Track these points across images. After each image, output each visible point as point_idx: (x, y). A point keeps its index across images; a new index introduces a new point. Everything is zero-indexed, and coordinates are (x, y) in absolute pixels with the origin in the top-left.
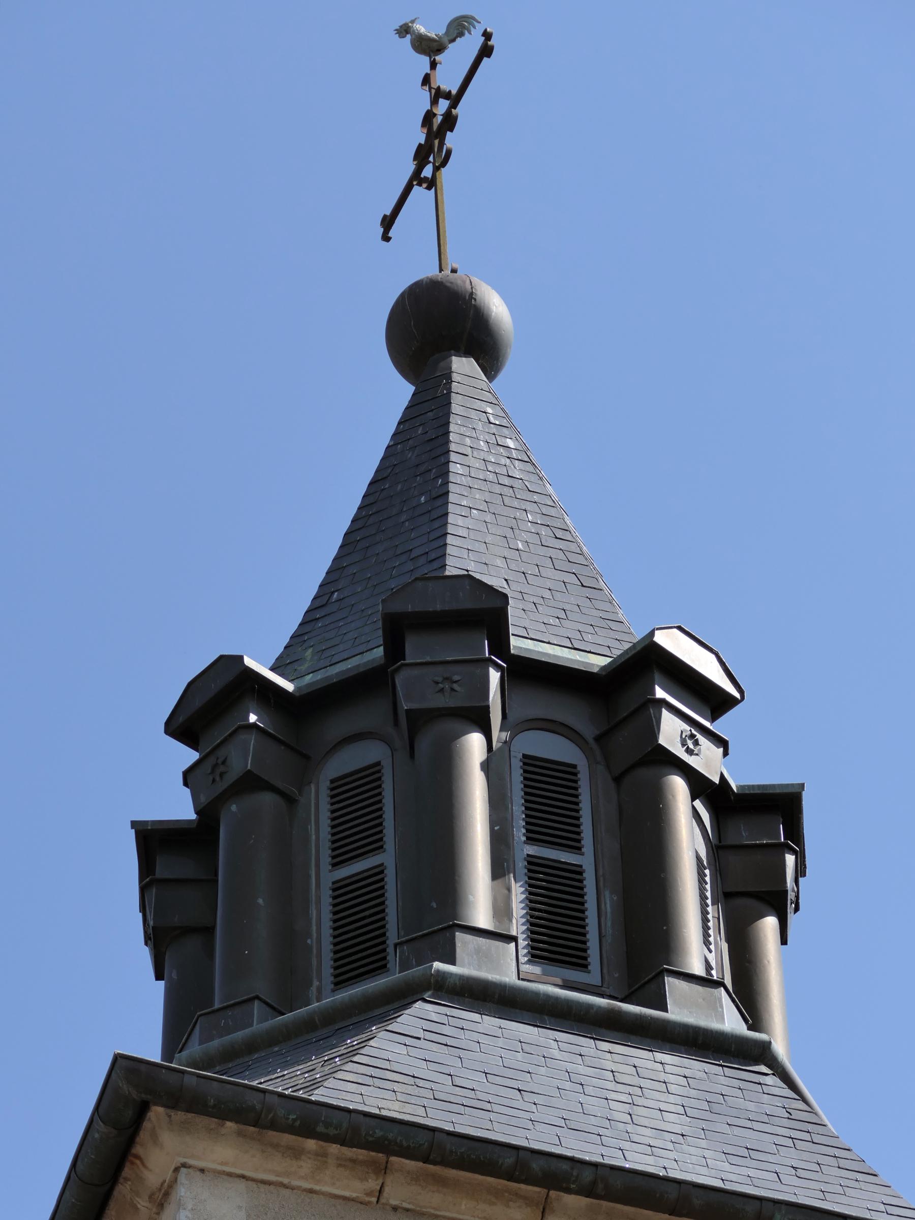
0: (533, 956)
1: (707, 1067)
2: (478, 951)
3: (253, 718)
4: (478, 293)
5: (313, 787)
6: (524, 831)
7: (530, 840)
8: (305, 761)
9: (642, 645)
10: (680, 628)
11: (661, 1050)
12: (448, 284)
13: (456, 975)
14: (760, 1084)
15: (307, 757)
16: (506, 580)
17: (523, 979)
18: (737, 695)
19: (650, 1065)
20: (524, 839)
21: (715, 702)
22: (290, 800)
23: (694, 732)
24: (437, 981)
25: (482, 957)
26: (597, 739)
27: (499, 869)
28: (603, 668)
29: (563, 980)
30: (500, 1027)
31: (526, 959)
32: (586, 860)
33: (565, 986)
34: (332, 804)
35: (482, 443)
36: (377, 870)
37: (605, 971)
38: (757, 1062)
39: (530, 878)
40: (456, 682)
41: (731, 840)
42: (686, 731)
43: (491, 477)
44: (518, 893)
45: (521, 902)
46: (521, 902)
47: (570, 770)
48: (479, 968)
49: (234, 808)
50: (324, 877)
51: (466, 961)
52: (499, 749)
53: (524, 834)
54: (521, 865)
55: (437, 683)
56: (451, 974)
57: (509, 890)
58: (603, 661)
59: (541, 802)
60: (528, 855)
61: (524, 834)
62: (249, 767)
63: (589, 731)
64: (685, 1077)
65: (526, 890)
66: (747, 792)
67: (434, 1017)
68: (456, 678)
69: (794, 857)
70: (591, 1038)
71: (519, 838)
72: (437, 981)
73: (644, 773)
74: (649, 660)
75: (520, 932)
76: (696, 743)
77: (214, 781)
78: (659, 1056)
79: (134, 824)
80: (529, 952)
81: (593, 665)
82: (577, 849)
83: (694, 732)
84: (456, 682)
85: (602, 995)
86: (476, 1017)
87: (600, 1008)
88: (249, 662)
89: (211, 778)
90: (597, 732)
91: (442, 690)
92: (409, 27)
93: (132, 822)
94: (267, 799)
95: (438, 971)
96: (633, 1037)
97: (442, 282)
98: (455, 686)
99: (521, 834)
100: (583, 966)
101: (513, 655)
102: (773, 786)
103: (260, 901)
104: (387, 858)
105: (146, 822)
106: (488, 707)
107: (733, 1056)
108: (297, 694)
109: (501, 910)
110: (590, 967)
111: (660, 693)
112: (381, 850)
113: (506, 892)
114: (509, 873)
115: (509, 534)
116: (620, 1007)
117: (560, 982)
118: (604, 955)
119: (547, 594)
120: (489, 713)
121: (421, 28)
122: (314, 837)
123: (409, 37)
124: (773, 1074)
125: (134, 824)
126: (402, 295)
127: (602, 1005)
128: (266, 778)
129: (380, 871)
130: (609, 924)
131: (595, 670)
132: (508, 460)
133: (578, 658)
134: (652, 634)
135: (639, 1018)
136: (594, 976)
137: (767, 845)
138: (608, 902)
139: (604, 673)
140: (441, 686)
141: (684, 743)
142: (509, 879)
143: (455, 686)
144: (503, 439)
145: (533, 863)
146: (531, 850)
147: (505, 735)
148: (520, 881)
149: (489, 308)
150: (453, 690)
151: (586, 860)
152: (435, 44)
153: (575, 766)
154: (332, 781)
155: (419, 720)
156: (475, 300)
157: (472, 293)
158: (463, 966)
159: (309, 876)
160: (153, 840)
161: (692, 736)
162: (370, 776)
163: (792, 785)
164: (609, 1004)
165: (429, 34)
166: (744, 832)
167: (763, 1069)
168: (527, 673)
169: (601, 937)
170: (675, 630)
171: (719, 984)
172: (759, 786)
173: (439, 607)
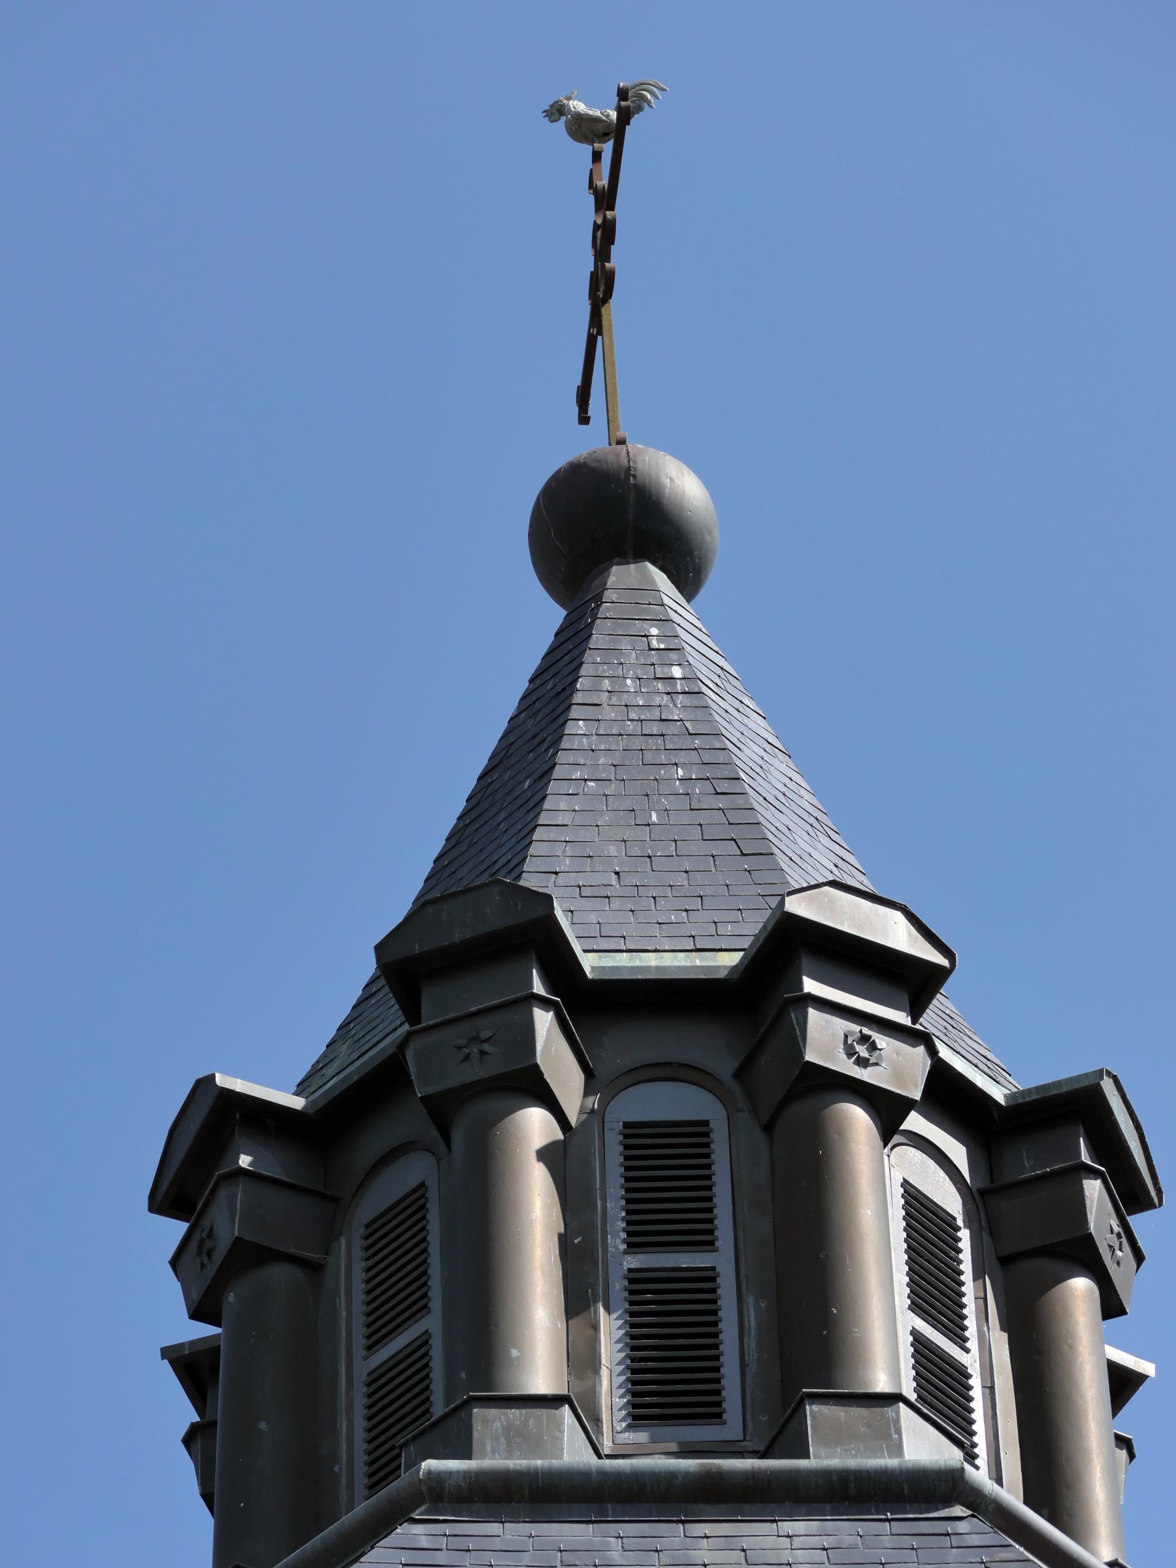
0: (635, 1418)
1: (860, 1527)
2: (507, 1430)
3: (245, 1161)
4: (640, 466)
5: (343, 1241)
6: (623, 1235)
7: (633, 1247)
8: (331, 1203)
9: (773, 922)
10: (834, 884)
11: (791, 1516)
12: (594, 465)
13: (458, 1472)
14: (948, 1534)
15: (334, 1200)
16: (617, 873)
17: (608, 1457)
18: (944, 962)
19: (770, 1542)
20: (623, 1247)
21: (914, 982)
22: (314, 1268)
23: (866, 1031)
24: (430, 1488)
25: (513, 1438)
26: (739, 1074)
27: (577, 1300)
28: (734, 969)
29: (680, 1443)
30: (531, 1536)
31: (624, 1424)
32: (721, 1260)
33: (683, 1453)
34: (368, 1259)
35: (629, 682)
36: (419, 1343)
37: (748, 1417)
38: (948, 1503)
39: (631, 1303)
40: (486, 1040)
41: (1009, 1176)
42: (853, 1033)
43: (631, 727)
44: (610, 1330)
45: (617, 1342)
46: (617, 1342)
47: (699, 1130)
48: (510, 1455)
49: (231, 1297)
50: (357, 1366)
51: (489, 1449)
52: (582, 1125)
53: (624, 1241)
54: (618, 1287)
55: (460, 1048)
56: (450, 1473)
57: (596, 1327)
58: (732, 959)
59: (648, 1190)
60: (630, 1270)
61: (624, 1241)
62: (236, 1234)
63: (724, 1066)
64: (824, 1549)
65: (626, 1322)
66: (1021, 1101)
67: (424, 1542)
68: (486, 1034)
69: (1099, 1181)
70: (677, 1522)
71: (616, 1247)
72: (430, 1488)
73: (799, 1109)
74: (793, 944)
75: (615, 1385)
76: (873, 1047)
77: (203, 1265)
78: (787, 1527)
79: (166, 1353)
80: (629, 1414)
81: (718, 967)
82: (709, 1244)
83: (866, 1031)
84: (486, 1040)
85: (741, 1454)
86: (494, 1528)
87: (687, 1474)
88: (221, 1080)
89: (198, 1261)
90: (736, 1064)
91: (467, 1057)
92: (563, 106)
93: (1125, 1313)
94: (279, 1274)
95: (429, 1473)
96: (746, 1507)
97: (585, 463)
98: (486, 1047)
99: (618, 1241)
100: (716, 1417)
101: (593, 981)
102: (1058, 1084)
103: (263, 1425)
104: (432, 1323)
105: (181, 1345)
106: (537, 1066)
107: (910, 1502)
108: (311, 1111)
109: (581, 1359)
110: (724, 1416)
111: (810, 986)
112: (426, 1310)
113: (592, 1331)
114: (595, 1302)
115: (639, 803)
116: (719, 1467)
117: (674, 1447)
118: (748, 1391)
119: (681, 879)
120: (541, 1074)
121: (578, 106)
122: (344, 1314)
123: (563, 119)
124: (973, 1516)
125: (166, 1353)
126: (538, 499)
127: (691, 1470)
128: (267, 1244)
129: (424, 1341)
130: (753, 1345)
131: (722, 975)
132: (666, 697)
133: (698, 963)
134: (782, 903)
135: (752, 1475)
136: (732, 1428)
137: (1054, 1174)
138: (752, 1312)
139: (736, 976)
140: (466, 1051)
141: (850, 1052)
142: (596, 1312)
143: (486, 1047)
144: (666, 669)
145: (635, 1279)
146: (634, 1261)
147: (593, 1102)
148: (616, 1311)
149: (659, 485)
150: (483, 1053)
151: (721, 1260)
152: (600, 126)
153: (706, 1123)
154: (367, 1226)
155: (442, 1111)
156: (635, 476)
157: (629, 469)
158: (483, 1457)
159: (336, 1373)
160: (216, 1120)
161: (864, 1039)
162: (413, 1205)
163: (1086, 1075)
164: (701, 1465)
165: (591, 113)
166: (1027, 1161)
167: (959, 1510)
168: (593, 1007)
169: (743, 1366)
170: (827, 888)
171: (895, 1398)
172: (1037, 1089)
173: (457, 937)
